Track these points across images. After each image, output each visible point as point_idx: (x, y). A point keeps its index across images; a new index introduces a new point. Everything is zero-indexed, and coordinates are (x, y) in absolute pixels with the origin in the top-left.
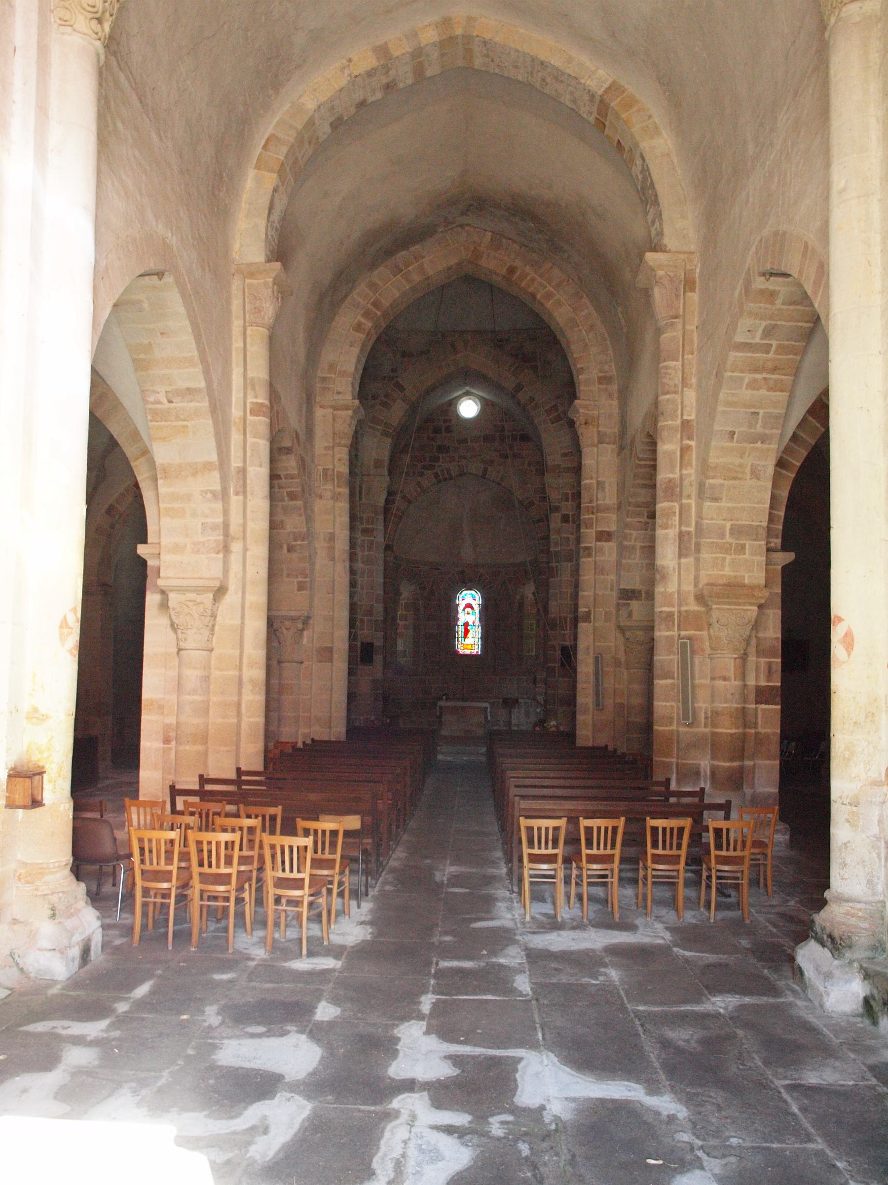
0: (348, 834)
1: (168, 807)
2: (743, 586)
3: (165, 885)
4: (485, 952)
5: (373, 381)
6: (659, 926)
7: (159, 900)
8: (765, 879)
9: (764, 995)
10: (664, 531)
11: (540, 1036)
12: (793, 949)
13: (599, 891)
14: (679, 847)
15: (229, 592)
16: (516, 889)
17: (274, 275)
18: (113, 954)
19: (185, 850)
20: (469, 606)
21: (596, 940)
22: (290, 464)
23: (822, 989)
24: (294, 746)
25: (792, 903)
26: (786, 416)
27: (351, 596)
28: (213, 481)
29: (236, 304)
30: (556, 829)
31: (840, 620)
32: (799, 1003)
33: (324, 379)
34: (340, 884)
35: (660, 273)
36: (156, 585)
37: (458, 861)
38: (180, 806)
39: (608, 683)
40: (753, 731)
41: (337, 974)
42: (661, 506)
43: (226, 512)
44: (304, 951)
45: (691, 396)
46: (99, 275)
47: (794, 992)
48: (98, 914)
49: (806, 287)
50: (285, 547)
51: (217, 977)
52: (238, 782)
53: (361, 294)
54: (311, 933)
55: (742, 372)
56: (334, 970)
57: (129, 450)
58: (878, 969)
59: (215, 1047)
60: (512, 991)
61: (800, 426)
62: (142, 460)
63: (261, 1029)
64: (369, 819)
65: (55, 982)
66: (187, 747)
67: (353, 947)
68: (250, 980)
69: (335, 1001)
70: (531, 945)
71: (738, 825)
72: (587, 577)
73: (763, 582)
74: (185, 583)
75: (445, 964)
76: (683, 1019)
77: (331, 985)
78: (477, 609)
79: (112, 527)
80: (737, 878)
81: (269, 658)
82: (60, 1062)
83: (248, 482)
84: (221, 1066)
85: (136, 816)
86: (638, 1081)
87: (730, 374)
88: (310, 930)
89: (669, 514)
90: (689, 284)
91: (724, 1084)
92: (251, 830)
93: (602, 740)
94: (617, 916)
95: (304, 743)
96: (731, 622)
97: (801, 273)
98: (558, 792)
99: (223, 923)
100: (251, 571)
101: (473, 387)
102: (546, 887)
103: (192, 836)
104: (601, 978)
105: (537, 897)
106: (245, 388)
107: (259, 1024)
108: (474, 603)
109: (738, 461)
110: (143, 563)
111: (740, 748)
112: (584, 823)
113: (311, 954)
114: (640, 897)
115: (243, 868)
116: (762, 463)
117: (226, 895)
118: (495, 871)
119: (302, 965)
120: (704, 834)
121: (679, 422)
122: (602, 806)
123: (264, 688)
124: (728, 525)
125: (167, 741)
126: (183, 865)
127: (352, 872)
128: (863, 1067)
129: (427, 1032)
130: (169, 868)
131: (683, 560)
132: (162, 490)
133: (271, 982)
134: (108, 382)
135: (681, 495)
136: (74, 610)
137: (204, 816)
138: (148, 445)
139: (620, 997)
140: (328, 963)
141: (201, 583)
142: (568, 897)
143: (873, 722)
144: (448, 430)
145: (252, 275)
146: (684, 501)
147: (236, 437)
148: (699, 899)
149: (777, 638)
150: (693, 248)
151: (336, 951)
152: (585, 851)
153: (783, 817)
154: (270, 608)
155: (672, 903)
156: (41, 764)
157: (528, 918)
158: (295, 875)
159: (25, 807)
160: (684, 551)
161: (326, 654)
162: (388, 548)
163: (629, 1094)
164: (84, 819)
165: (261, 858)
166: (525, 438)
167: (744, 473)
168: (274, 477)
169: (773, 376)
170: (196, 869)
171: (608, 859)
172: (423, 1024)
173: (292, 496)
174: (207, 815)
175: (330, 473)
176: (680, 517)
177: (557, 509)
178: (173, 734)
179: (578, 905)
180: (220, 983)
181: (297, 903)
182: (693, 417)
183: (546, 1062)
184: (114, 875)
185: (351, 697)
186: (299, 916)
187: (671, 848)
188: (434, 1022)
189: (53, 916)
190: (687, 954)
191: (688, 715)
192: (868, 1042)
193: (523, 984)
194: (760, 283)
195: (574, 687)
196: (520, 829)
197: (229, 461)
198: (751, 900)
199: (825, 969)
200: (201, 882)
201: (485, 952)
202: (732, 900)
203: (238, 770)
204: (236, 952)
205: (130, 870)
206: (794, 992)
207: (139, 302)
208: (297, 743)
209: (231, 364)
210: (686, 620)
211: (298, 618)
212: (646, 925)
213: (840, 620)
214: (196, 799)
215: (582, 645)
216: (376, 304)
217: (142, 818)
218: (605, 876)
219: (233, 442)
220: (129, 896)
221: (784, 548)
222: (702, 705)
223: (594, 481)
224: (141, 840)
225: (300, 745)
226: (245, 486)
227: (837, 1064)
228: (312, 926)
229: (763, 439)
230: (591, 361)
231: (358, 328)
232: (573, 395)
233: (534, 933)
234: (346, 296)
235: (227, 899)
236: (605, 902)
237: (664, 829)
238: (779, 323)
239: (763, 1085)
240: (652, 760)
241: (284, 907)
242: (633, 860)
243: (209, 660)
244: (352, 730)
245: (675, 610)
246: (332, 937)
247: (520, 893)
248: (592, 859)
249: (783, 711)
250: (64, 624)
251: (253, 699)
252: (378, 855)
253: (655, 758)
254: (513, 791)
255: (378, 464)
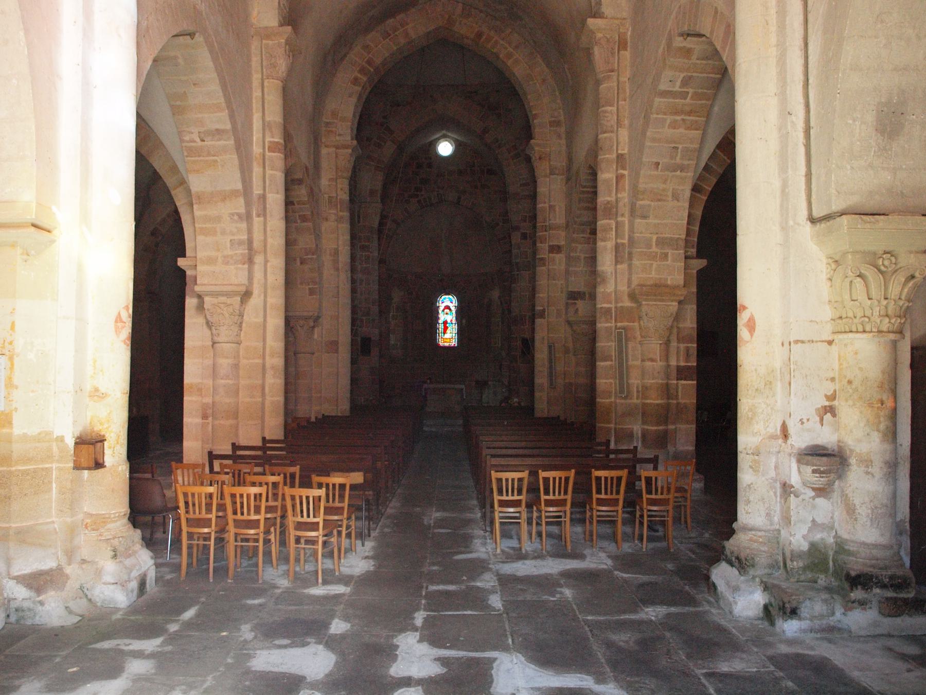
0: (353, 487)
1: (207, 470)
2: (666, 286)
3: (206, 530)
4: (465, 578)
5: (367, 126)
6: (603, 555)
7: (201, 542)
8: (685, 518)
9: (685, 605)
10: (603, 243)
11: (510, 641)
12: (708, 570)
13: (555, 529)
14: (618, 492)
15: (254, 296)
16: (488, 529)
17: (285, 36)
18: (164, 586)
19: (222, 502)
20: (447, 307)
21: (552, 567)
22: (302, 192)
23: (731, 599)
24: (308, 420)
25: (707, 535)
26: (700, 150)
27: (353, 301)
28: (239, 205)
29: (255, 61)
30: (520, 480)
31: (744, 308)
32: (713, 611)
33: (327, 124)
34: (348, 527)
35: (599, 35)
36: (193, 291)
37: (442, 508)
38: (217, 468)
39: (560, 367)
40: (675, 402)
41: (346, 597)
42: (601, 223)
43: (250, 231)
44: (320, 581)
45: (624, 135)
46: (142, 34)
47: (709, 602)
48: (151, 554)
49: (716, 44)
50: (298, 260)
51: (250, 602)
52: (263, 448)
53: (356, 55)
54: (325, 566)
55: (665, 114)
56: (343, 595)
57: (170, 181)
58: (775, 582)
59: (249, 657)
60: (488, 607)
61: (710, 158)
62: (180, 189)
63: (286, 642)
64: (369, 476)
65: (117, 609)
66: (222, 422)
67: (359, 577)
68: (276, 604)
69: (346, 618)
70: (502, 572)
71: (663, 475)
72: (542, 282)
73: (682, 283)
74: (217, 289)
75: (433, 588)
76: (622, 626)
77: (342, 606)
78: (453, 309)
79: (157, 245)
80: (664, 517)
81: (287, 350)
82: (123, 671)
83: (268, 206)
84: (256, 671)
85: (181, 477)
86: (588, 673)
87: (655, 116)
88: (324, 564)
89: (607, 229)
90: (622, 45)
91: (656, 674)
92: (275, 485)
93: (556, 411)
94: (569, 548)
95: (316, 418)
96: (657, 315)
97: (712, 32)
98: (521, 452)
99: (254, 559)
100: (271, 278)
101: (448, 130)
102: (511, 527)
103: (227, 490)
104: (558, 596)
105: (506, 535)
106: (264, 130)
107: (284, 637)
108: (451, 305)
109: (662, 186)
110: (183, 272)
111: (665, 415)
112: (543, 474)
113: (325, 582)
114: (587, 533)
115: (269, 516)
116: (681, 188)
117: (256, 537)
118: (471, 516)
119: (318, 591)
120: (637, 483)
121: (614, 156)
122: (557, 461)
123: (283, 373)
124: (654, 238)
125: (205, 417)
126: (220, 514)
127: (357, 518)
128: (763, 658)
129: (420, 641)
130: (209, 516)
131: (619, 266)
132: (198, 213)
133: (294, 605)
134: (151, 125)
135: (617, 215)
136: (127, 308)
137: (236, 476)
138: (185, 176)
139: (573, 610)
140: (340, 589)
141: (230, 288)
142: (530, 534)
143: (771, 389)
144: (430, 166)
145: (268, 37)
146: (620, 219)
147: (257, 170)
148: (634, 533)
149: (693, 328)
150: (625, 14)
151: (345, 580)
152: (543, 497)
153: (698, 470)
154: (286, 311)
155: (613, 538)
156: (102, 433)
157: (499, 551)
158: (312, 519)
159: (89, 469)
160: (619, 259)
161: (333, 346)
162: (382, 261)
163: (581, 683)
164: (140, 479)
165: (284, 508)
166: (490, 172)
167: (666, 196)
168: (288, 203)
169: (691, 118)
170: (231, 517)
171: (562, 503)
172: (417, 634)
173: (304, 219)
174: (239, 475)
175: (334, 200)
176: (616, 231)
177: (517, 228)
178: (210, 411)
179: (538, 540)
180: (250, 608)
181: (312, 542)
182: (626, 151)
183: (515, 661)
184: (165, 524)
185: (354, 381)
186: (315, 553)
187: (612, 493)
188: (426, 632)
189: (115, 556)
190: (625, 575)
191: (624, 389)
192: (768, 639)
193: (496, 601)
194: (679, 42)
195: (533, 372)
196: (491, 481)
197: (251, 188)
198: (675, 534)
199: (734, 584)
200: (236, 527)
201: (465, 578)
202: (660, 533)
203: (264, 439)
204: (264, 582)
205: (177, 519)
206: (709, 602)
207: (176, 57)
208: (310, 418)
209: (252, 110)
210: (622, 313)
211: (310, 317)
212: (592, 555)
213: (744, 308)
214: (229, 462)
215: (538, 337)
216: (369, 62)
217: (186, 479)
218: (560, 517)
219: (254, 174)
220: (177, 541)
221: (699, 255)
222: (635, 381)
223: (547, 205)
224: (185, 495)
225: (313, 419)
226: (265, 208)
227: (744, 656)
228: (325, 561)
229: (682, 168)
230: (544, 107)
231: (355, 81)
232: (529, 136)
233: (503, 562)
234: (345, 55)
235: (257, 541)
236: (560, 537)
237: (606, 478)
238: (694, 74)
239: (686, 674)
240: (595, 427)
241: (303, 546)
242: (581, 504)
243: (238, 352)
244: (354, 407)
245: (613, 306)
246: (342, 569)
247: (492, 532)
248: (549, 503)
249: (699, 386)
250: (119, 319)
251: (274, 382)
252: (378, 505)
253: (598, 425)
254: (485, 452)
255: (372, 192)
